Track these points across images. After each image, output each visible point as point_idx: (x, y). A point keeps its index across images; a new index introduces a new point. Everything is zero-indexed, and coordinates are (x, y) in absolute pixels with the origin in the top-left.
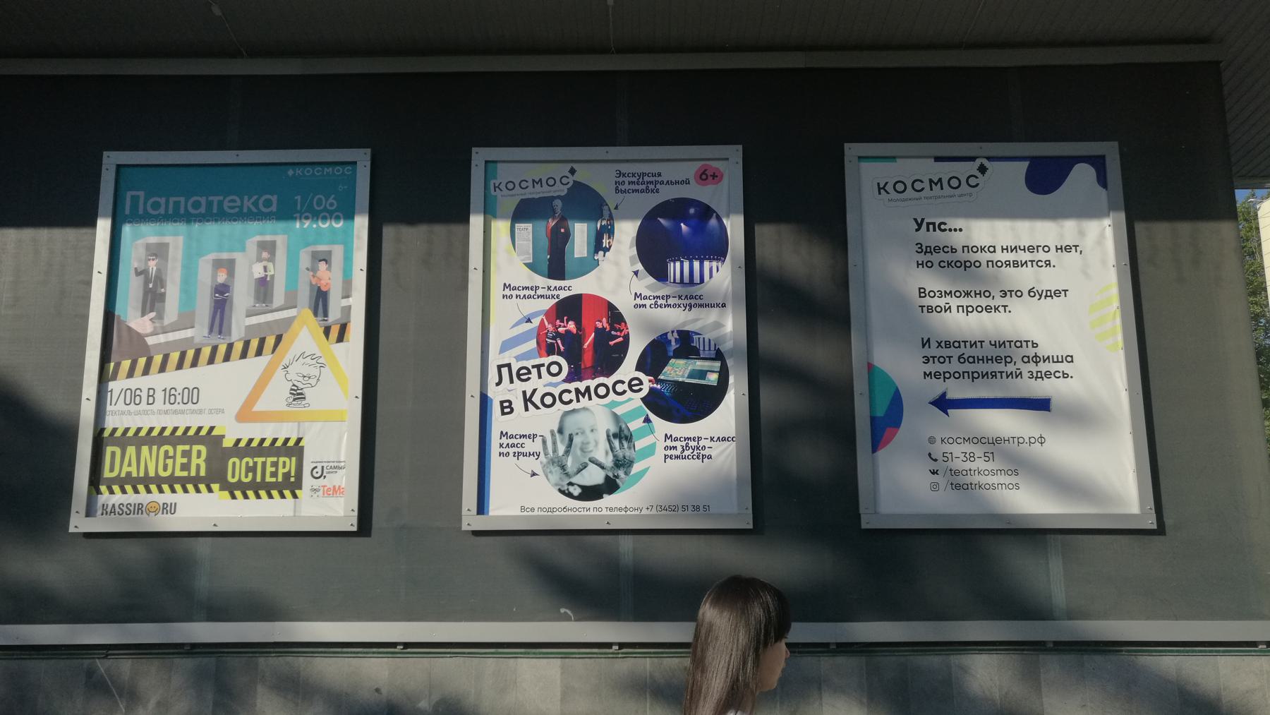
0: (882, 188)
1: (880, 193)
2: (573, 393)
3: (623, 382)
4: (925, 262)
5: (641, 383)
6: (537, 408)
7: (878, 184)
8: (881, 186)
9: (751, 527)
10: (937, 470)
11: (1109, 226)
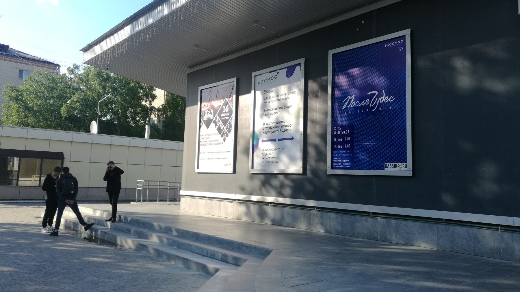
9: (411, 175)
11: (276, 67)
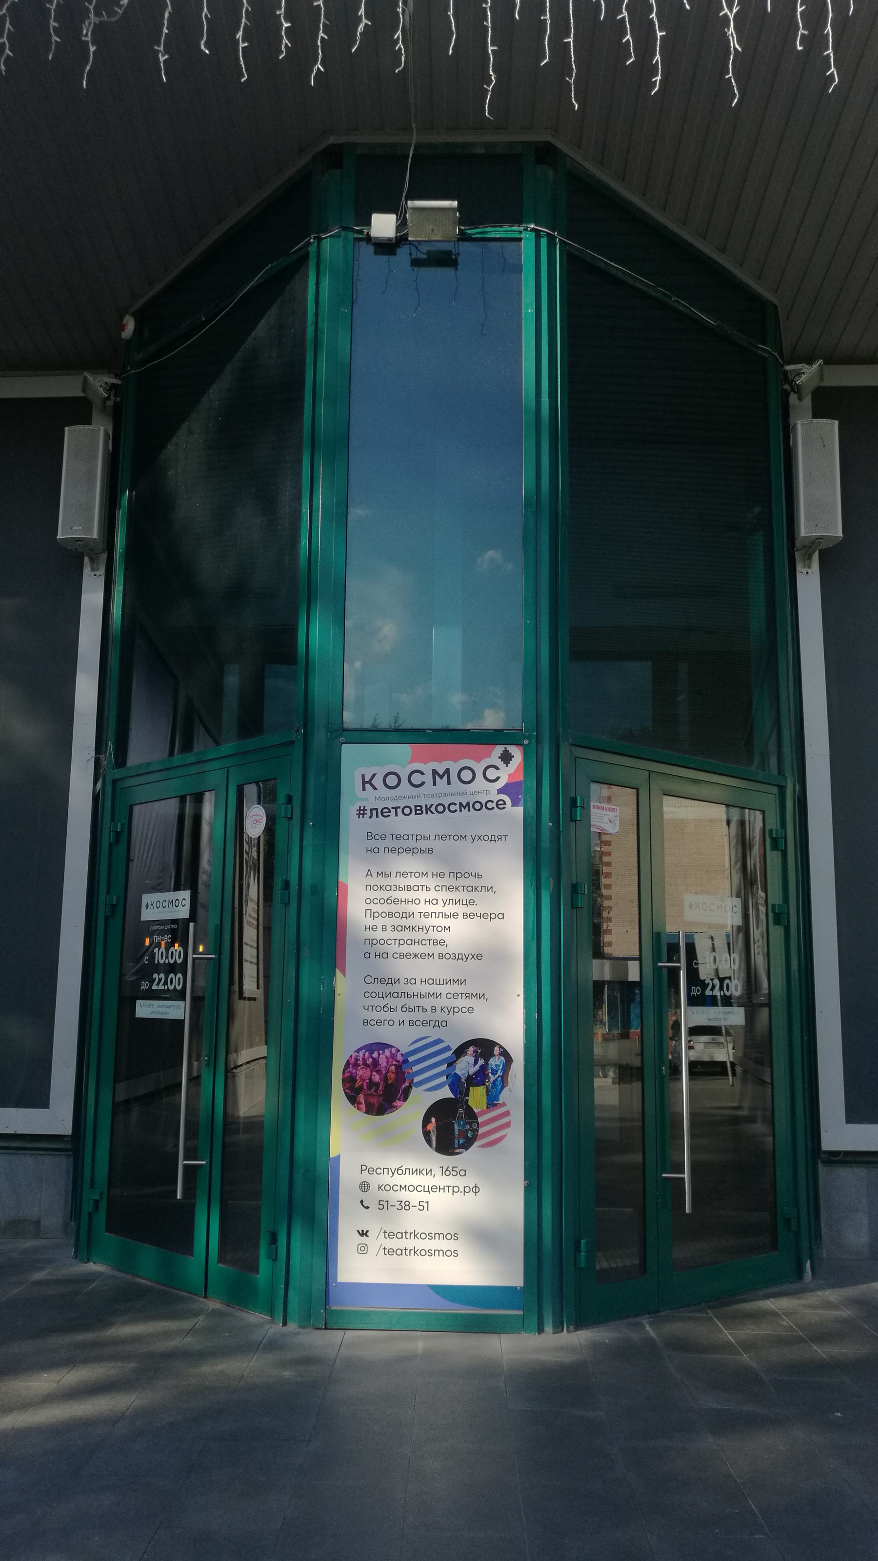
0: (367, 782)
1: (364, 789)
2: (458, 805)
4: (400, 918)
5: (505, 803)
6: (432, 813)
7: (363, 776)
8: (367, 779)
10: (367, 1231)
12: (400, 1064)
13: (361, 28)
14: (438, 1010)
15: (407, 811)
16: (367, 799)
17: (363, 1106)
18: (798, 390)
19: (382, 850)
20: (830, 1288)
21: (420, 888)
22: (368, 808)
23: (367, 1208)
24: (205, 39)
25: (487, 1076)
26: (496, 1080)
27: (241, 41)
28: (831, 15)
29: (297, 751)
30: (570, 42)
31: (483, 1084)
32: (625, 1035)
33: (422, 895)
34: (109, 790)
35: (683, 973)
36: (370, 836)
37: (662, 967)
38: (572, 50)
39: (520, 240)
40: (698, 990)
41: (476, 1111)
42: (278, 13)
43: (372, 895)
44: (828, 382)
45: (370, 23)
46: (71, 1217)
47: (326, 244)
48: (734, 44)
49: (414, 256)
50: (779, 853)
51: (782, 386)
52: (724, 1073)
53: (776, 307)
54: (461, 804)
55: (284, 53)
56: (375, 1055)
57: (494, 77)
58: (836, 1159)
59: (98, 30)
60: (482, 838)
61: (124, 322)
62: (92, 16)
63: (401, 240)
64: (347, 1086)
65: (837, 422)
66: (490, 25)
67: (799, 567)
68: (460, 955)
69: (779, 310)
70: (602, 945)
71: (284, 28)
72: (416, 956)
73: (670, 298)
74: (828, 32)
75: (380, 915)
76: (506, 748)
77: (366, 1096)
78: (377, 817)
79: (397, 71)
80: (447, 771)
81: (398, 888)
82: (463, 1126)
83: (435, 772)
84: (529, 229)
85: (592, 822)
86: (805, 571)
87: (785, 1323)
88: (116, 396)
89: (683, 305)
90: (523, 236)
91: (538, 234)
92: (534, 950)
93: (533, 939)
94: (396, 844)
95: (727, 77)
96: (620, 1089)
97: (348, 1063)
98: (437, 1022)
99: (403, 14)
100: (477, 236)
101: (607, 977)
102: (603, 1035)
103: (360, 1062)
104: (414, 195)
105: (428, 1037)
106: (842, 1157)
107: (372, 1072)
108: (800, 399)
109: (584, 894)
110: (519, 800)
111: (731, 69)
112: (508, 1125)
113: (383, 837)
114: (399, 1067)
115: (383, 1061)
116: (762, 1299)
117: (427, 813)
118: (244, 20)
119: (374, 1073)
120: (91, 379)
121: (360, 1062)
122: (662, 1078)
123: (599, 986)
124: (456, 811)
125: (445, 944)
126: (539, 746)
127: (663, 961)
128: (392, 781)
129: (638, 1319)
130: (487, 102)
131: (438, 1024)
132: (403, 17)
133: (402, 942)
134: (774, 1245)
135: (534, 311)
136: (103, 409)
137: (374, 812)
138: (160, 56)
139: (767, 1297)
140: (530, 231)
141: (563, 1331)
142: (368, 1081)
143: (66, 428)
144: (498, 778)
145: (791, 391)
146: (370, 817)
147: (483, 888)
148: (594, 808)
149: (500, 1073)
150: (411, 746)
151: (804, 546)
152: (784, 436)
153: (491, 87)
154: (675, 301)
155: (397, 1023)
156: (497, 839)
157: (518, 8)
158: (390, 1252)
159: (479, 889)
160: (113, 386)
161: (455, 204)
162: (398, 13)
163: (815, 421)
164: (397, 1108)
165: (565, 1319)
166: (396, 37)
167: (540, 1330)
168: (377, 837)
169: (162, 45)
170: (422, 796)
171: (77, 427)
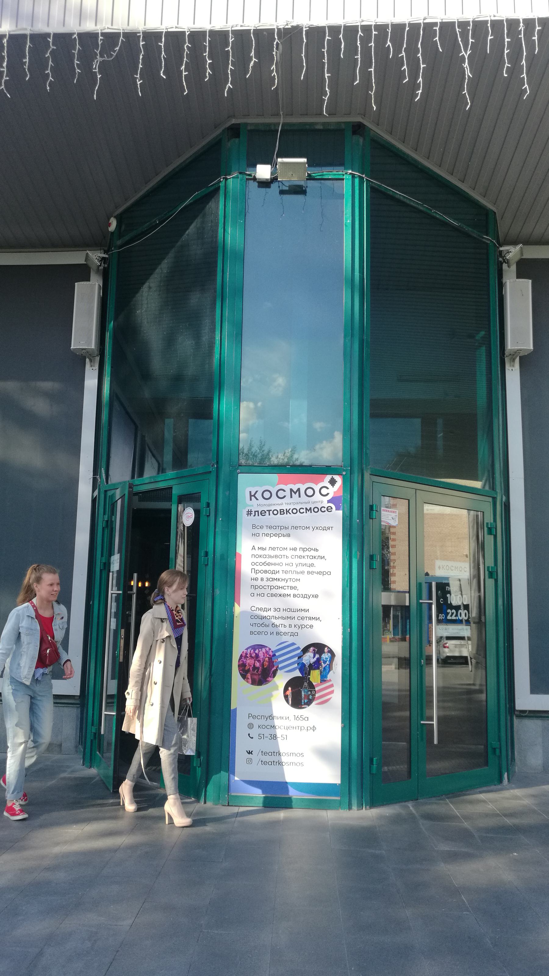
0: (253, 496)
1: (251, 500)
2: (305, 509)
3: (325, 507)
5: (332, 508)
6: (290, 514)
7: (250, 492)
8: (253, 494)
10: (252, 751)
12: (271, 657)
13: (252, 64)
14: (293, 626)
15: (275, 512)
16: (252, 506)
17: (250, 680)
18: (508, 262)
19: (261, 535)
20: (518, 788)
21: (283, 556)
22: (253, 510)
23: (252, 738)
24: (163, 70)
25: (320, 664)
26: (326, 666)
27: (184, 71)
28: (525, 54)
29: (213, 477)
30: (372, 71)
31: (318, 668)
32: (403, 639)
33: (284, 561)
34: (102, 496)
35: (435, 607)
36: (254, 526)
37: (422, 603)
38: (373, 76)
39: (343, 179)
40: (443, 616)
41: (314, 684)
42: (204, 54)
43: (255, 560)
44: (525, 256)
45: (257, 61)
46: (79, 742)
47: (230, 182)
48: (468, 73)
49: (281, 188)
50: (492, 536)
51: (498, 259)
52: (466, 663)
53: (495, 213)
54: (306, 509)
55: (208, 77)
56: (257, 651)
57: (329, 92)
58: (524, 715)
59: (102, 68)
60: (318, 528)
61: (110, 221)
62: (98, 57)
63: (274, 179)
64: (241, 669)
65: (530, 281)
66: (326, 62)
67: (507, 366)
68: (306, 595)
69: (497, 215)
70: (390, 583)
71: (208, 63)
72: (280, 595)
73: (431, 210)
74: (523, 64)
75: (260, 572)
76: (332, 477)
77: (252, 675)
78: (258, 515)
79: (272, 89)
80: (299, 490)
81: (270, 556)
82: (307, 692)
83: (291, 490)
84: (348, 173)
85: (382, 519)
86: (511, 369)
87: (490, 807)
88: (104, 263)
89: (439, 215)
90: (345, 177)
91: (353, 176)
92: (348, 593)
93: (347, 587)
94: (269, 531)
95: (463, 93)
96: (399, 672)
97: (241, 656)
98: (292, 633)
99: (276, 55)
100: (318, 177)
101: (393, 603)
102: (390, 639)
103: (248, 655)
104: (280, 155)
105: (287, 642)
106: (528, 713)
107: (255, 661)
108: (509, 266)
109: (377, 561)
110: (340, 506)
111: (466, 88)
112: (332, 692)
113: (262, 527)
114: (270, 659)
115: (261, 655)
116: (478, 794)
117: (287, 514)
118: (185, 59)
119: (256, 662)
120: (91, 254)
121: (248, 655)
122: (421, 666)
123: (386, 609)
124: (304, 512)
125: (297, 589)
126: (352, 475)
127: (423, 599)
128: (267, 495)
129: (406, 803)
130: (325, 106)
131: (293, 634)
132: (276, 57)
133: (272, 587)
134: (486, 764)
135: (350, 221)
136: (98, 271)
137: (257, 513)
138: (138, 81)
139: (481, 792)
140: (349, 174)
141: (363, 809)
142: (253, 666)
143: (76, 284)
144: (328, 494)
145: (503, 262)
146: (254, 516)
147: (319, 557)
148: (383, 511)
149: (328, 663)
150: (278, 475)
151: (510, 354)
152: (499, 290)
153: (327, 98)
154: (434, 212)
155: (269, 634)
156: (327, 529)
157: (342, 51)
158: (265, 763)
159: (317, 557)
160: (103, 258)
161: (304, 160)
162: (273, 55)
163: (518, 280)
164: (269, 681)
165: (364, 802)
166: (272, 69)
167: (350, 808)
168: (258, 527)
169: (139, 74)
170: (284, 504)
171: (83, 283)
